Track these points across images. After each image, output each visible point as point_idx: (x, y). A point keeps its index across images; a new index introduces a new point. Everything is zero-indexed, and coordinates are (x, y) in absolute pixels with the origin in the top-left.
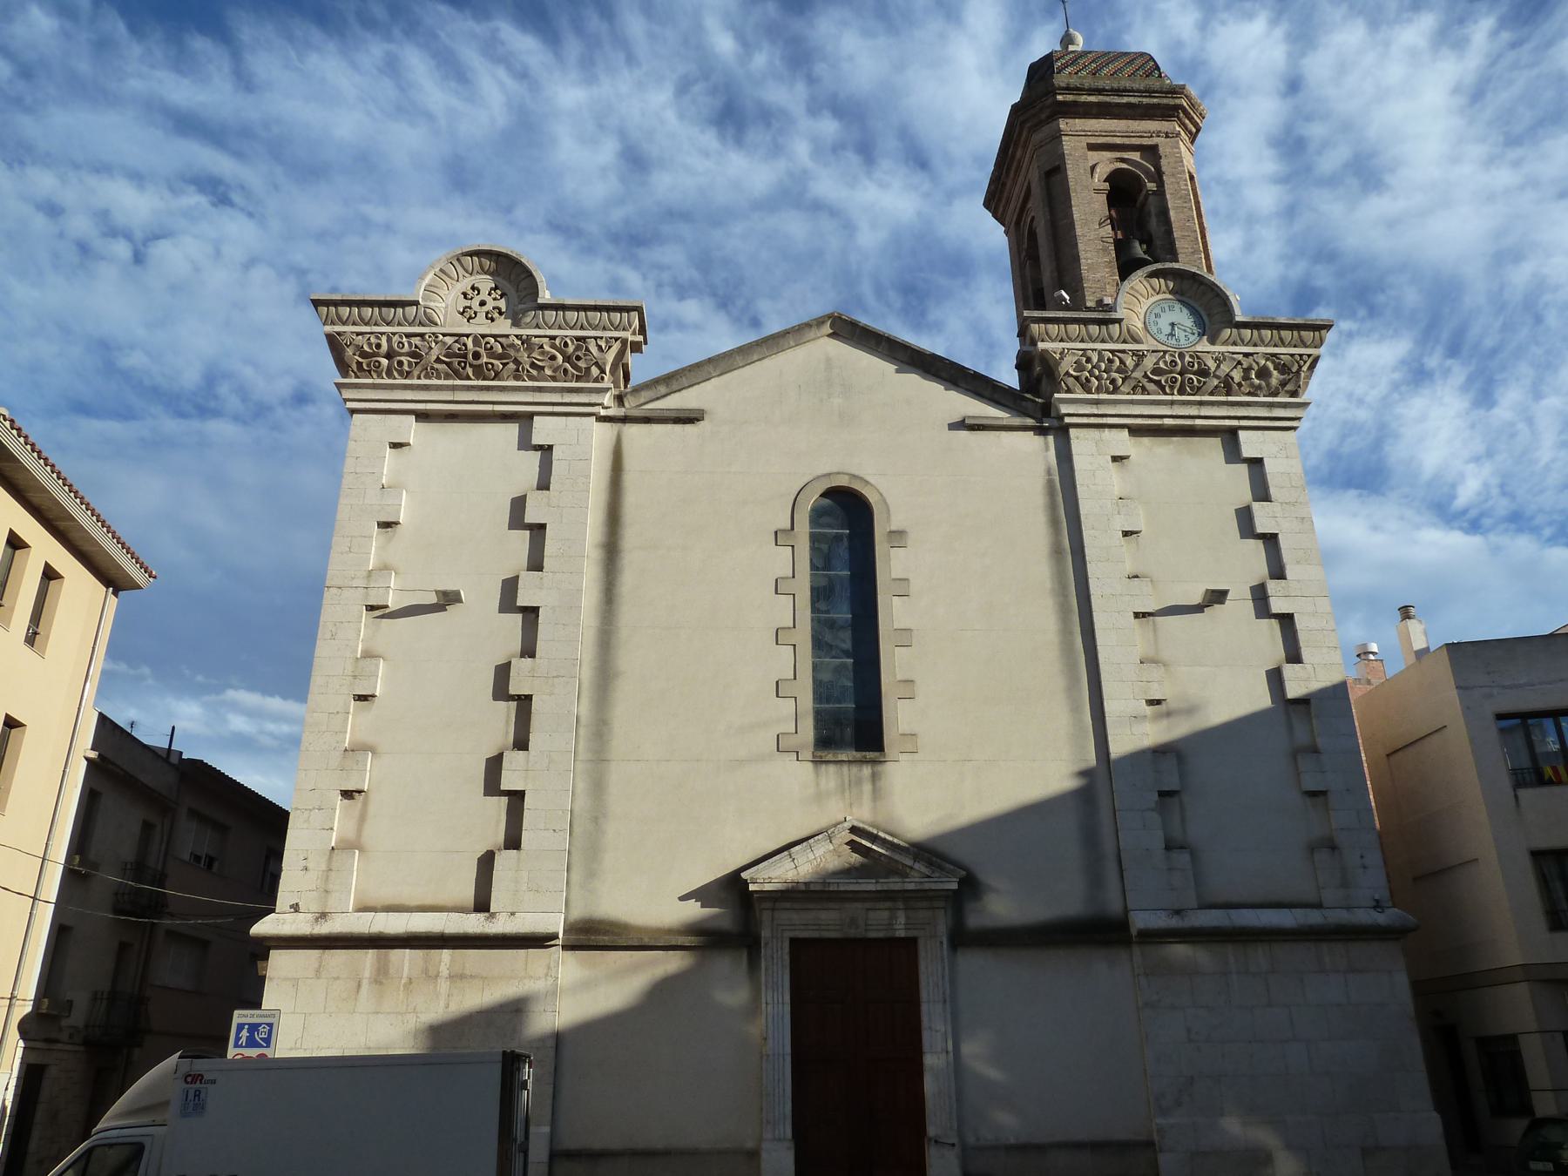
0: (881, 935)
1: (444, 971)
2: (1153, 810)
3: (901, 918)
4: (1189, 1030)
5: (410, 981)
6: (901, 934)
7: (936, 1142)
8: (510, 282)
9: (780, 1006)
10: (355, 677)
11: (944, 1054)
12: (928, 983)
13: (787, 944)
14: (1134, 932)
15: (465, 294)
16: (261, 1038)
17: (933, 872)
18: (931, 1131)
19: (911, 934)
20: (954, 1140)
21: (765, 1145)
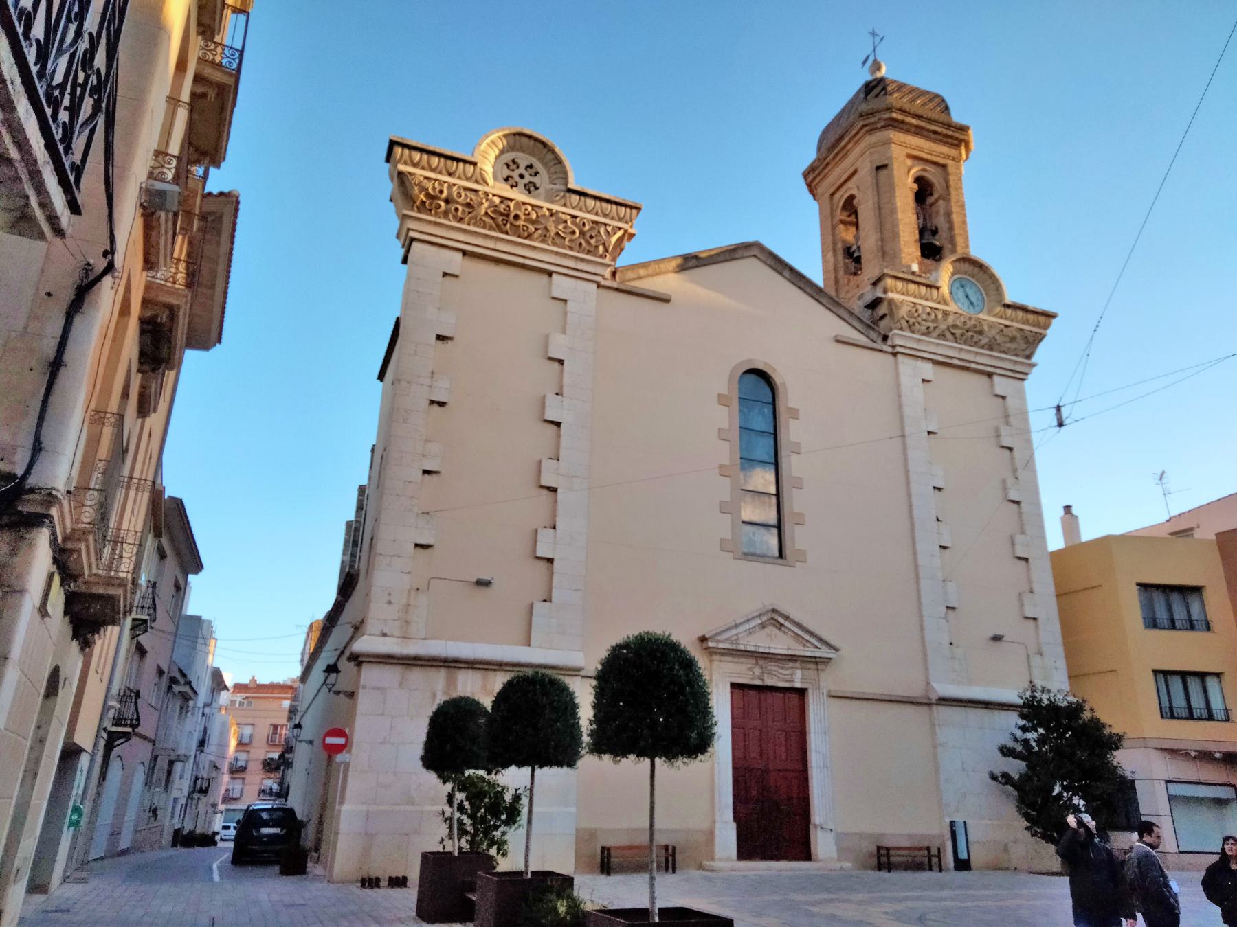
4: (963, 763)
19: (805, 686)
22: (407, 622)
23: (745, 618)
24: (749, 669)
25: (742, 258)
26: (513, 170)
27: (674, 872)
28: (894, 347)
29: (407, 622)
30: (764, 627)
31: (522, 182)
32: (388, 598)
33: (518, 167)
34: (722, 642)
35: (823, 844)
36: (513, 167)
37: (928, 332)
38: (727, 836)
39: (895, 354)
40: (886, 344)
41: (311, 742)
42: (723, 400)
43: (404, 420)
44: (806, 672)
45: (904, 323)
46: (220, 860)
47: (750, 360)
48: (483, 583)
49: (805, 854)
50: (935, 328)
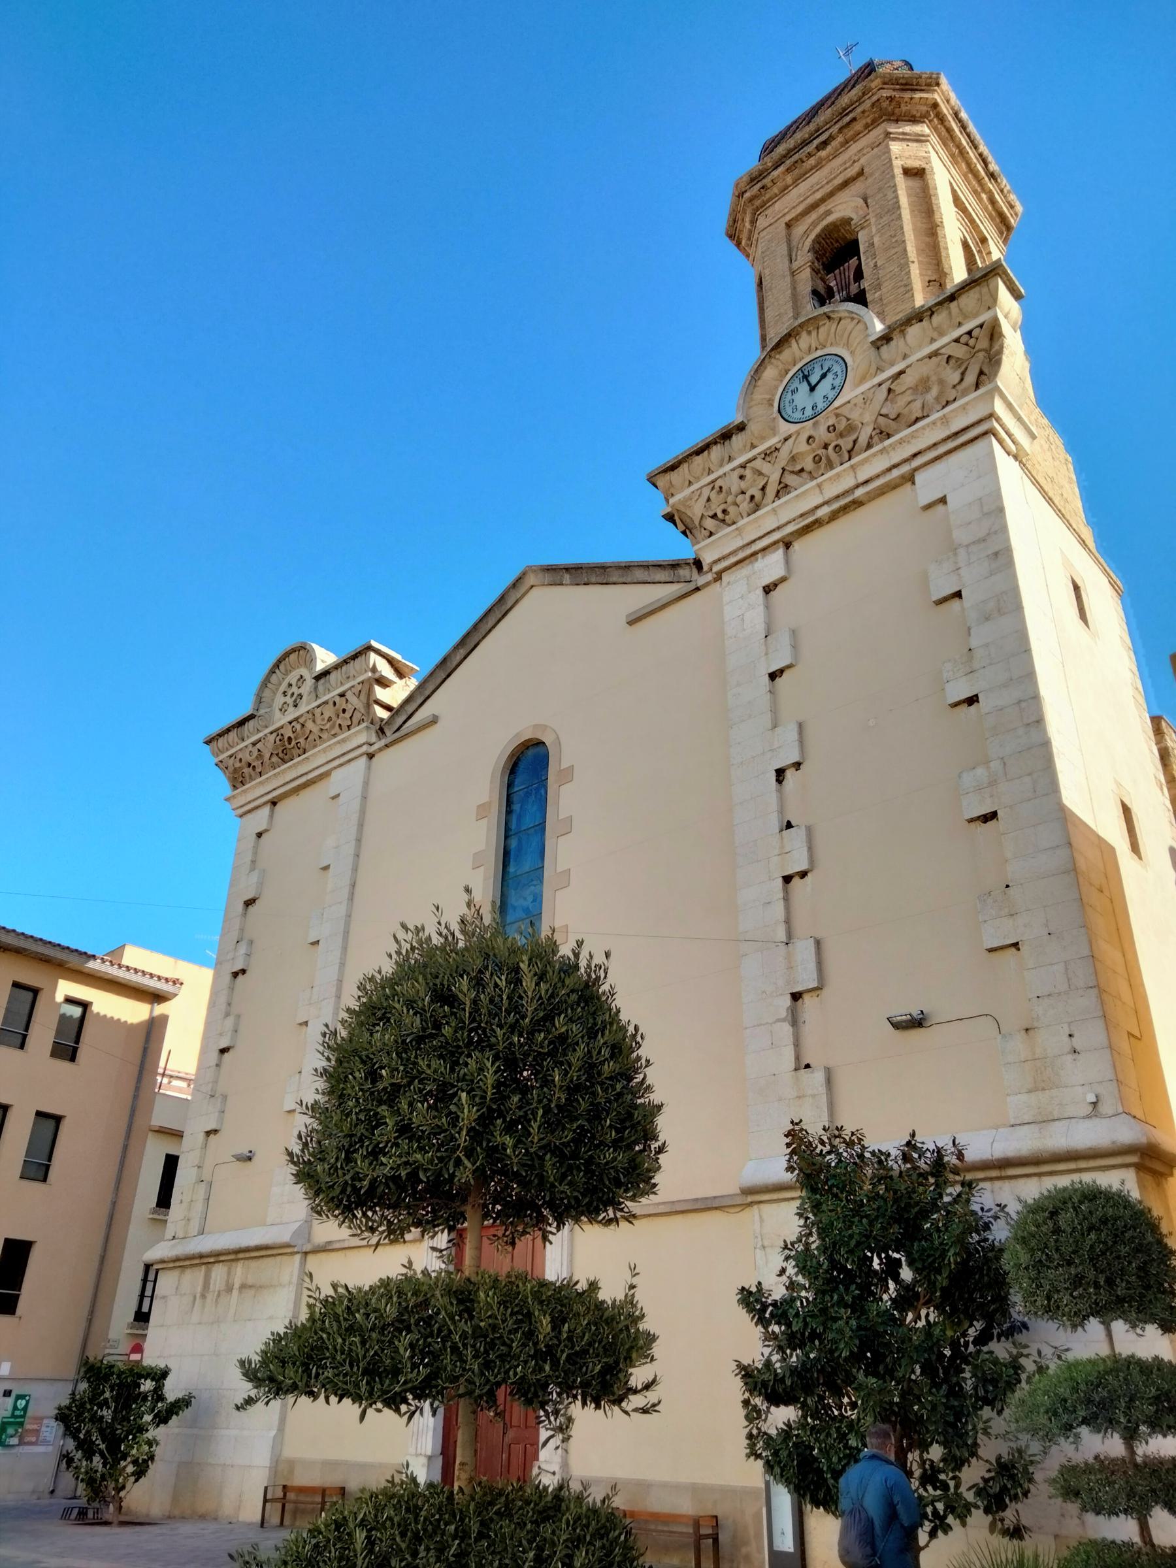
2: (784, 1020)
5: (219, 1292)
25: (517, 602)
37: (756, 505)
45: (710, 523)
50: (763, 489)
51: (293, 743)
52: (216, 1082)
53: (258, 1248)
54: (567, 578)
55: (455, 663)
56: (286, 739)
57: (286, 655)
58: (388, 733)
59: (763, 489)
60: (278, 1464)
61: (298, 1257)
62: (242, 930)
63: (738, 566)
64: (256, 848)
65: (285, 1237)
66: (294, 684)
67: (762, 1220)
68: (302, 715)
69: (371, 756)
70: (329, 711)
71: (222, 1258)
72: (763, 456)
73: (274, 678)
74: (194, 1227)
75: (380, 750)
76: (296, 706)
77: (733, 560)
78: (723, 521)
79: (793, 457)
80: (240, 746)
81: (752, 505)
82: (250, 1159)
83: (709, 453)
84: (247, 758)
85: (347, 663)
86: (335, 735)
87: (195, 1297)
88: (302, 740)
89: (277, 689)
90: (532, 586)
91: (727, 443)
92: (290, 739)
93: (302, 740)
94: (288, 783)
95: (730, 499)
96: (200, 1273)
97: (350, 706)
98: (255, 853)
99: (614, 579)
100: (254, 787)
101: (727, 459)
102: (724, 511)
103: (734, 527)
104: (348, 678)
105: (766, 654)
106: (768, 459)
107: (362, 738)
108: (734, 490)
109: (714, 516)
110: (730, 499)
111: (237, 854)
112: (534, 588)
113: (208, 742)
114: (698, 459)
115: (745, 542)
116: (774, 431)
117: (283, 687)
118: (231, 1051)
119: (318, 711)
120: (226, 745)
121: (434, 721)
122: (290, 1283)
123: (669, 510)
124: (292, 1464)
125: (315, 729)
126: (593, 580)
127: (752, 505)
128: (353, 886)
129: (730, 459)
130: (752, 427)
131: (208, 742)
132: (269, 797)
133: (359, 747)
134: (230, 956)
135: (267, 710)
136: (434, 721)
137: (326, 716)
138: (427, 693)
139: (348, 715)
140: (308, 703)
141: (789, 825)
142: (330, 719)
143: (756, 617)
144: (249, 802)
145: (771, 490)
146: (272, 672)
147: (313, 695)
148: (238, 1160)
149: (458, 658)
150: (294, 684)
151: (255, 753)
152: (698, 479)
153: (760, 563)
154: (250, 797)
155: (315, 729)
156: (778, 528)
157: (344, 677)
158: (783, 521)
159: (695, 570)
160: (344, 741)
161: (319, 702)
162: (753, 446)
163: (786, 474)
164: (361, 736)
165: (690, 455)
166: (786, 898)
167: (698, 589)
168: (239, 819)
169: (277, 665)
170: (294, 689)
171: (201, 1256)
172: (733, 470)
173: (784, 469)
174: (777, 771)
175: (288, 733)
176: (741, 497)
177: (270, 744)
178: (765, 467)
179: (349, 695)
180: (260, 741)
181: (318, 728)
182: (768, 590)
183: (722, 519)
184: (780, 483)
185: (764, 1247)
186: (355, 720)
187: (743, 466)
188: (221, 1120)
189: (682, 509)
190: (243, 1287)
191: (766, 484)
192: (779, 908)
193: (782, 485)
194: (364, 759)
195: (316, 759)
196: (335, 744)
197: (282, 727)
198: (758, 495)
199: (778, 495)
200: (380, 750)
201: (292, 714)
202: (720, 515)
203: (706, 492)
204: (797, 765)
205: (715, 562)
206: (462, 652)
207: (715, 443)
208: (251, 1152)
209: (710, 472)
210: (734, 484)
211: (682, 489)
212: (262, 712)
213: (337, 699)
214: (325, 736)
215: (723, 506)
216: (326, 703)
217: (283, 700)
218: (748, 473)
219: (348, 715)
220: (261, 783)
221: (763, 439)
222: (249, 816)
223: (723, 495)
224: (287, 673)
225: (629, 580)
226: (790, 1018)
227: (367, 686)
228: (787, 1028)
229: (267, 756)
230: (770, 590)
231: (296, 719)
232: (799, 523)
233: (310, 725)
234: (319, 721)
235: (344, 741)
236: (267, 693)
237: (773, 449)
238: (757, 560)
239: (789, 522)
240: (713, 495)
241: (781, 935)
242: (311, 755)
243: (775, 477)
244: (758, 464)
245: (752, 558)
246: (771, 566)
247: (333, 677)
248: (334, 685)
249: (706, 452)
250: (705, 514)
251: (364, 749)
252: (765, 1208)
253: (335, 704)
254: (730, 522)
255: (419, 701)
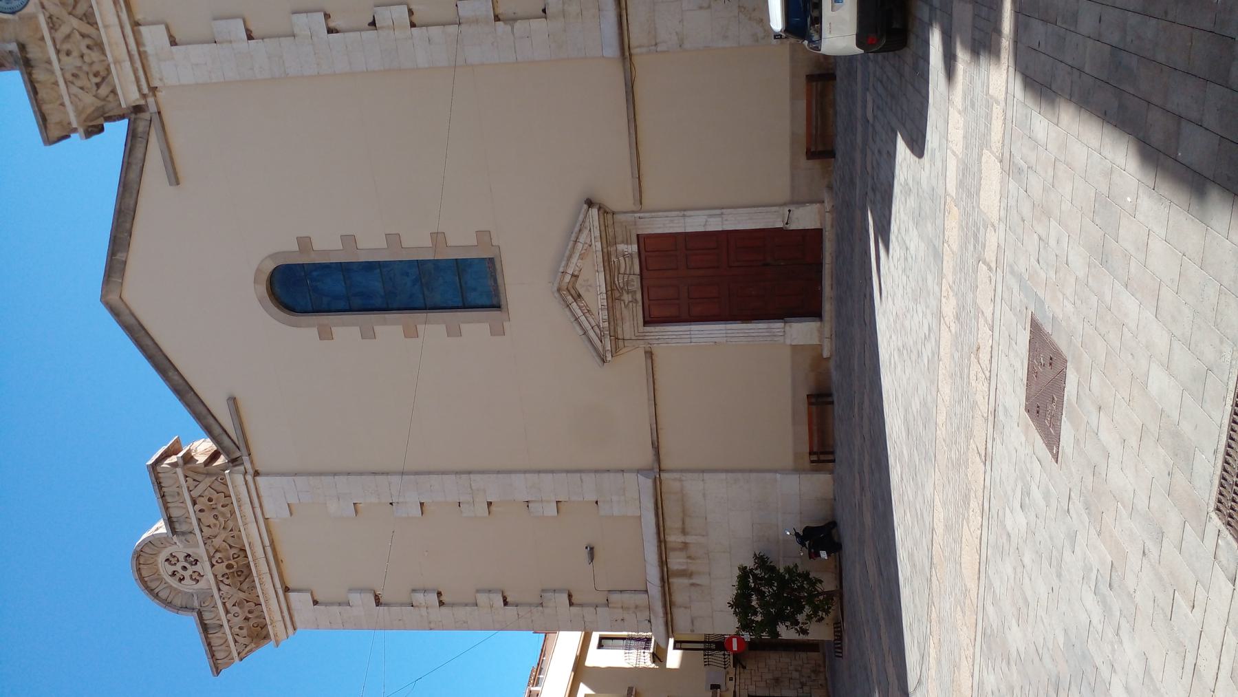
0: (636, 261)
1: (681, 539)
2: (513, 28)
3: (621, 247)
4: (701, 8)
5: (689, 557)
6: (635, 248)
7: (787, 224)
8: (159, 552)
9: (692, 333)
10: (215, 42)
11: (723, 216)
12: (671, 227)
13: (648, 329)
14: (818, 343)
15: (181, 580)
16: (811, 48)
17: (586, 228)
18: (779, 225)
19: (634, 239)
20: (786, 209)
21: (788, 342)
22: (636, 607)
23: (575, 325)
24: (626, 306)
25: (133, 314)
26: (194, 572)
27: (830, 395)
28: (144, 96)
29: (636, 607)
30: (579, 296)
31: (187, 574)
32: (619, 621)
33: (191, 576)
34: (604, 347)
35: (805, 218)
36: (173, 561)
37: (98, 46)
38: (801, 332)
39: (153, 90)
40: (147, 105)
41: (692, 631)
42: (325, 334)
43: (465, 622)
44: (619, 239)
45: (104, 91)
46: (630, 633)
47: (260, 301)
48: (591, 551)
49: (814, 237)
50: (83, 36)
51: (232, 562)
52: (530, 605)
53: (657, 515)
54: (120, 256)
55: (181, 381)
56: (228, 571)
57: (142, 580)
58: (238, 454)
59: (83, 36)
60: (797, 470)
61: (664, 475)
62: (402, 605)
63: (147, 71)
64: (326, 604)
65: (649, 482)
66: (174, 568)
67: (640, 46)
68: (207, 550)
69: (257, 473)
70: (208, 518)
71: (664, 558)
72: (53, 31)
73: (163, 595)
74: (641, 599)
75: (252, 462)
76: (196, 561)
77: (141, 73)
78: (104, 79)
79: (61, 3)
80: (228, 626)
81: (95, 48)
82: (592, 549)
83: (38, 82)
84: (238, 621)
85: (164, 496)
86: (233, 513)
87: (693, 585)
88: (232, 551)
89: (175, 589)
90: (120, 297)
91: (33, 63)
92: (229, 567)
93: (232, 551)
94: (270, 570)
95: (86, 68)
96: (675, 581)
97: (206, 493)
98: (332, 604)
99: (132, 202)
100: (269, 610)
101: (48, 66)
102: (96, 75)
103: (112, 67)
104: (178, 494)
105: (231, 42)
106: (57, 26)
107: (239, 479)
108: (78, 63)
109: (98, 85)
110: (86, 68)
111: (331, 625)
112: (123, 297)
113: (217, 670)
114: (42, 93)
115: (128, 58)
116: (33, 17)
117: (173, 582)
118: (505, 594)
119: (205, 529)
120: (223, 647)
121: (233, 401)
122: (681, 480)
123: (81, 130)
124: (797, 456)
125: (223, 535)
126: (128, 225)
127: (95, 48)
128: (374, 473)
129: (49, 62)
130: (23, 38)
131: (217, 670)
132: (280, 592)
133: (246, 484)
134: (424, 611)
135: (195, 597)
136: (233, 401)
137: (212, 521)
138: (204, 412)
139: (215, 496)
140: (197, 546)
141: (373, 24)
142: (216, 517)
143: (197, 52)
144: (283, 617)
145: (86, 29)
146: (156, 596)
147: (189, 537)
148: (592, 561)
149: (176, 378)
150: (174, 568)
151: (236, 609)
152: (61, 97)
153: (149, 48)
154: (278, 617)
155: (223, 535)
156: (122, 28)
157: (177, 498)
158: (116, 20)
159: (142, 115)
160: (239, 500)
161: (197, 531)
162: (42, 39)
163: (74, 12)
164: (237, 481)
165: (36, 100)
166: (427, 25)
167: (159, 113)
168: (298, 631)
169: (150, 591)
170: (178, 568)
171: (662, 579)
172: (59, 60)
173: (70, 14)
174: (328, 32)
175: (221, 568)
176: (86, 59)
177: (232, 591)
178: (64, 30)
179: (195, 493)
180: (224, 604)
181: (222, 531)
182: (173, 43)
183: (103, 77)
184: (81, 19)
185: (656, 44)
186: (221, 488)
187: (58, 52)
188: (561, 591)
189: (84, 116)
190: (684, 532)
191: (78, 30)
192: (434, 31)
193: (84, 18)
194: (258, 478)
195: (252, 535)
196: (240, 511)
197: (215, 576)
198: (88, 41)
199: (93, 24)
200: (252, 462)
201: (205, 567)
202: (98, 80)
203: (74, 90)
204: (327, 16)
205: (140, 90)
206: (171, 373)
207: (30, 75)
208: (587, 548)
209: (56, 83)
210: (72, 62)
211: (66, 113)
212: (196, 604)
213: (198, 507)
214: (231, 524)
215: (91, 76)
216: (199, 520)
217: (187, 581)
218: (66, 47)
219: (215, 496)
220: (266, 601)
221: (37, 28)
222: (296, 619)
223: (82, 75)
224: (161, 580)
225: (136, 186)
226: (511, 22)
227: (189, 473)
228: (518, 25)
229: (242, 595)
230: (174, 41)
231: (210, 558)
232: (121, 8)
233: (217, 542)
234: (216, 530)
235: (239, 500)
236: (178, 601)
237: (50, 20)
238: (145, 52)
239: (119, 17)
240: (79, 83)
241: (452, 29)
242: (248, 539)
243: (75, 22)
244: (59, 35)
245: (143, 56)
246: (154, 37)
247: (175, 513)
248: (184, 511)
249: (36, 85)
250: (94, 93)
251: (249, 478)
252: (633, 43)
253: (201, 511)
254: (106, 72)
255: (211, 421)
